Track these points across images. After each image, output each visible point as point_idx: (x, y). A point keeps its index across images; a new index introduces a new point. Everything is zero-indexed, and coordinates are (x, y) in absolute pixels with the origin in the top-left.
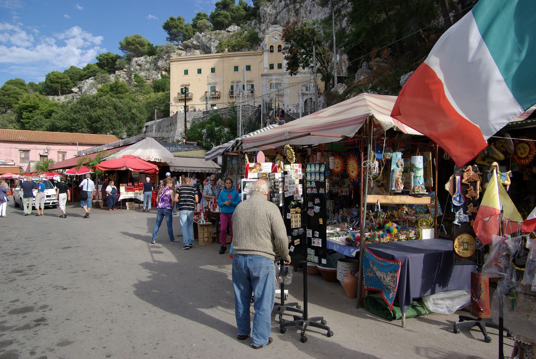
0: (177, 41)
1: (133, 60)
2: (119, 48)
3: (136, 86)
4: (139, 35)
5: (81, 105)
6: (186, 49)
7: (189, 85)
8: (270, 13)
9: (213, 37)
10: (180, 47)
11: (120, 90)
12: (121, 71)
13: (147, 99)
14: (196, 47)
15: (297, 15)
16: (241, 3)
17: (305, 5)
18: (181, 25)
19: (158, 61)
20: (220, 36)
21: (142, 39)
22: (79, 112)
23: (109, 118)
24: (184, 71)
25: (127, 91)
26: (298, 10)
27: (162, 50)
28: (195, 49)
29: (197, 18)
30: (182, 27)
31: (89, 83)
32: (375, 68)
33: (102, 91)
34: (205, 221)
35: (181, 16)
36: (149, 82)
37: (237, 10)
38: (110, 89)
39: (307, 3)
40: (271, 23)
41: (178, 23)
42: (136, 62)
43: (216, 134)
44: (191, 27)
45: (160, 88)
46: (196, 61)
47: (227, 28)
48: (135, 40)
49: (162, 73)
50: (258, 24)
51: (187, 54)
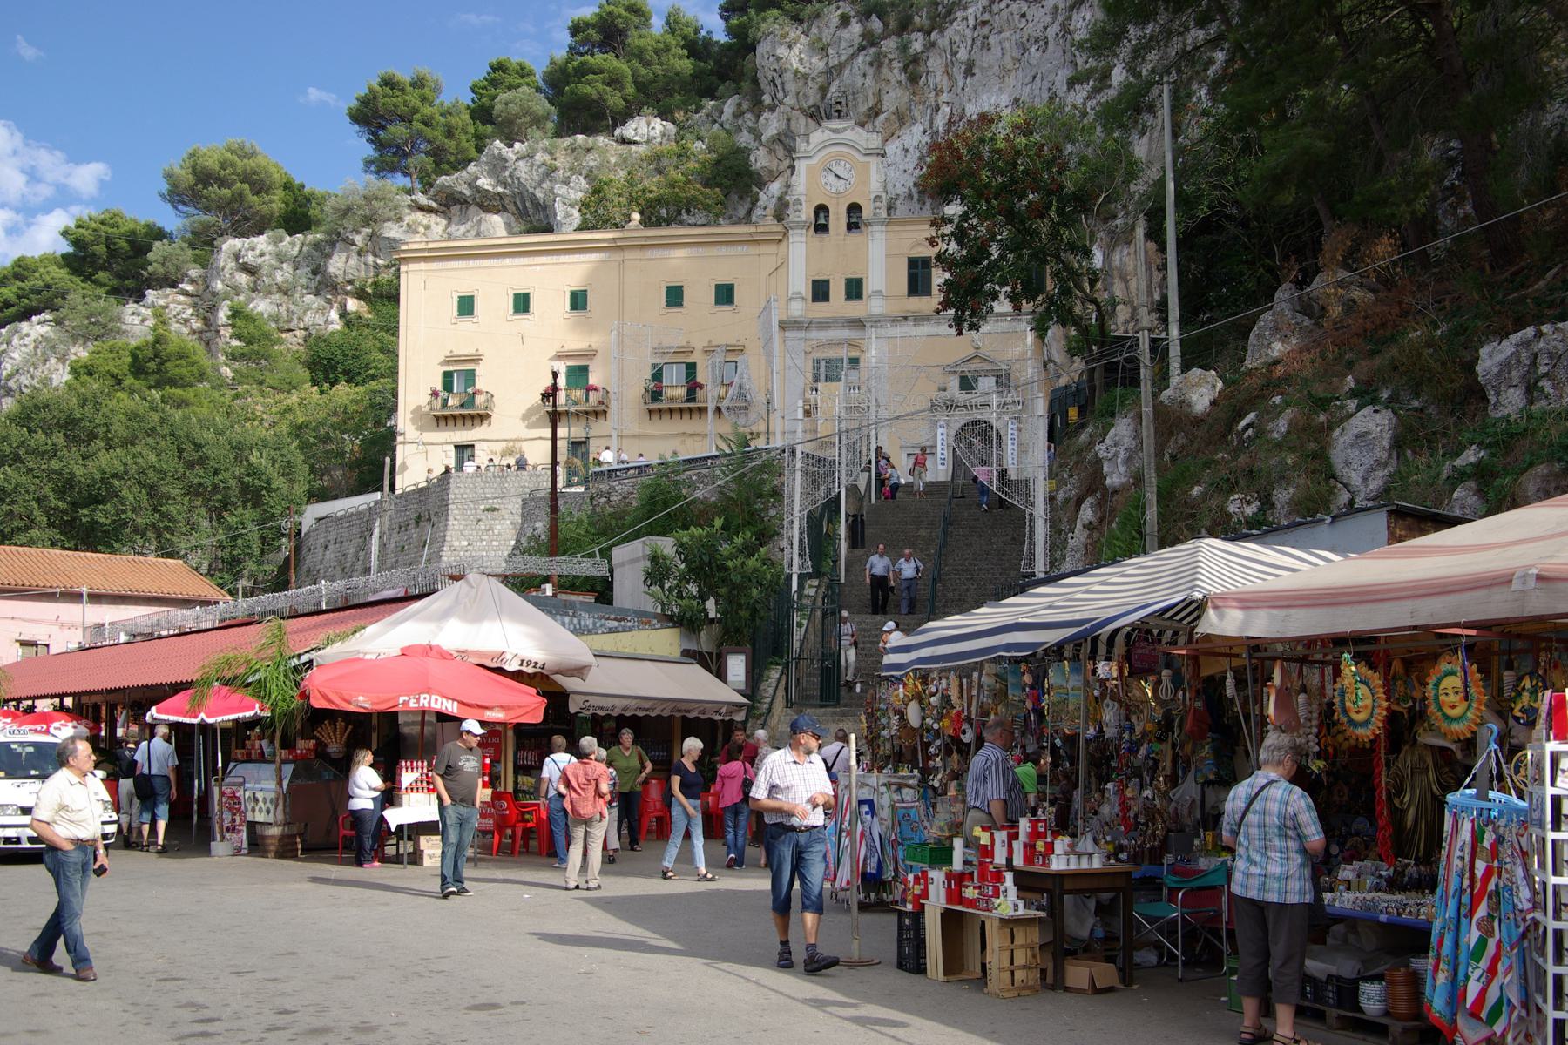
0: (406, 174)
1: (224, 247)
2: (162, 196)
3: (234, 357)
4: (248, 145)
5: (30, 431)
6: (447, 206)
7: (476, 360)
8: (802, 70)
9: (562, 161)
10: (423, 199)
11: (173, 370)
12: (168, 291)
13: (289, 410)
14: (488, 203)
15: (914, 79)
16: (673, 23)
17: (946, 42)
18: (426, 110)
19: (329, 256)
20: (591, 160)
21: (261, 160)
22: (17, 458)
23: (152, 490)
24: (456, 300)
25: (202, 376)
26: (915, 60)
27: (349, 209)
28: (487, 209)
29: (494, 83)
30: (432, 118)
31: (34, 335)
32: (1336, 311)
33: (90, 374)
34: (1021, 904)
35: (425, 70)
36: (293, 341)
37: (657, 51)
38: (132, 365)
39: (957, 32)
40: (802, 111)
41: (413, 98)
42: (237, 256)
43: (730, 564)
44: (466, 117)
45: (334, 368)
46: (507, 261)
47: (615, 126)
48: (232, 165)
49: (343, 306)
50: (748, 115)
51: (453, 228)
